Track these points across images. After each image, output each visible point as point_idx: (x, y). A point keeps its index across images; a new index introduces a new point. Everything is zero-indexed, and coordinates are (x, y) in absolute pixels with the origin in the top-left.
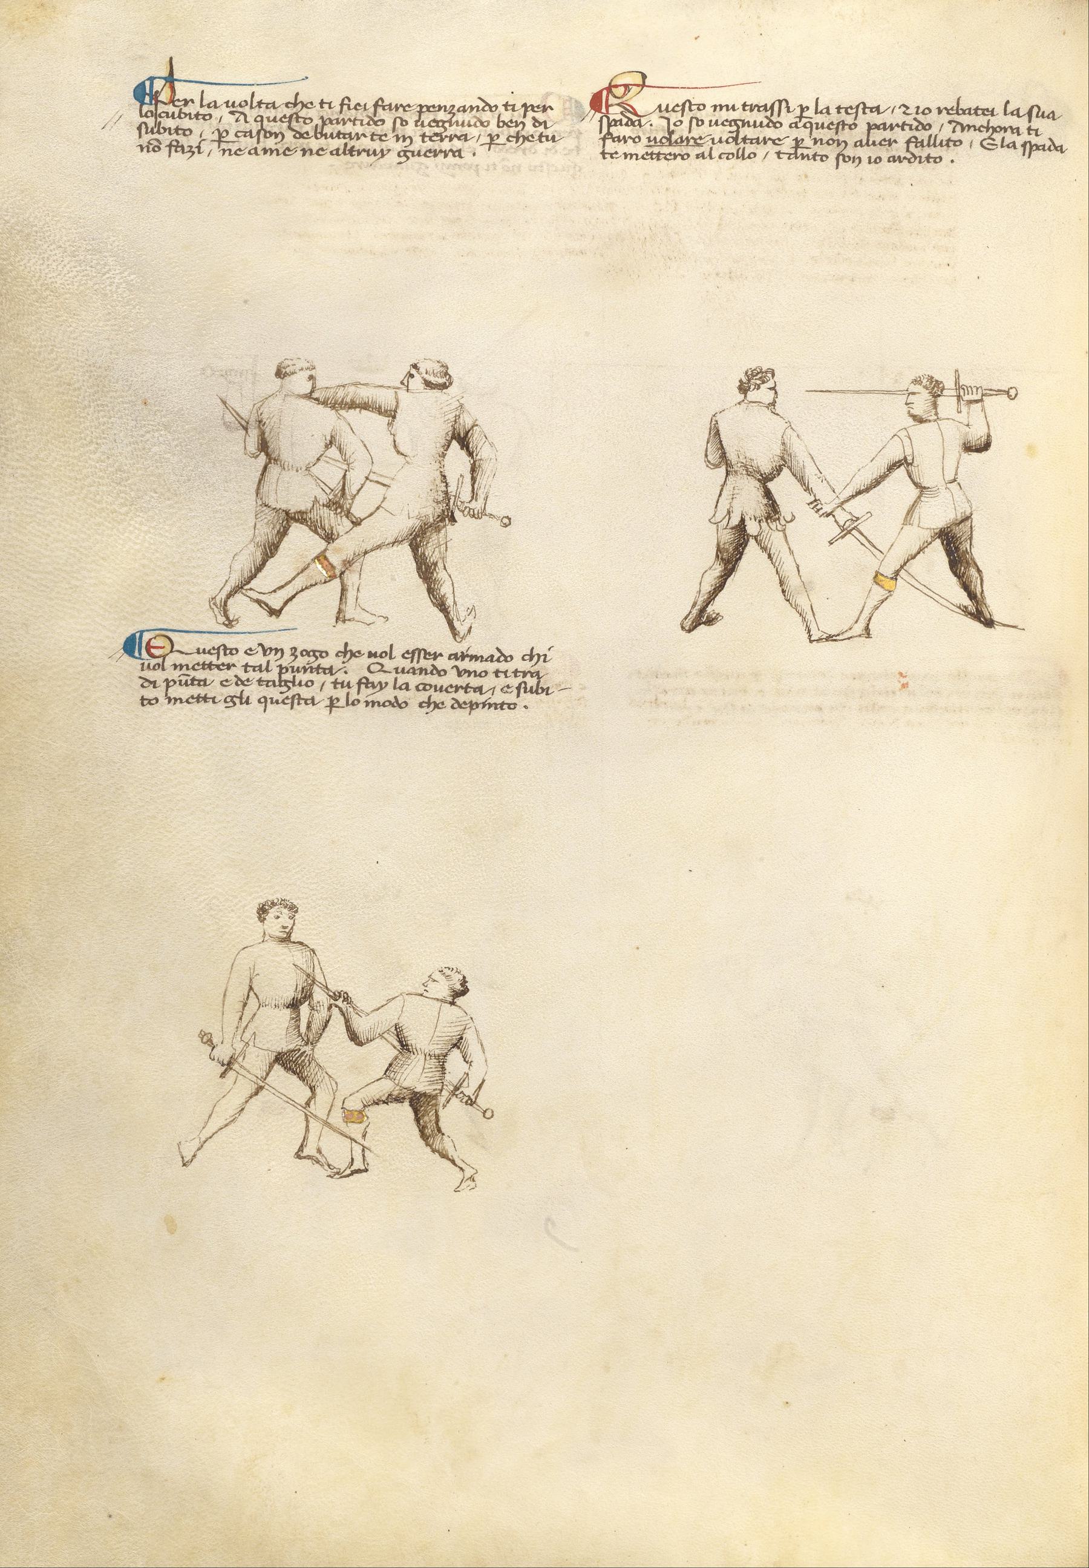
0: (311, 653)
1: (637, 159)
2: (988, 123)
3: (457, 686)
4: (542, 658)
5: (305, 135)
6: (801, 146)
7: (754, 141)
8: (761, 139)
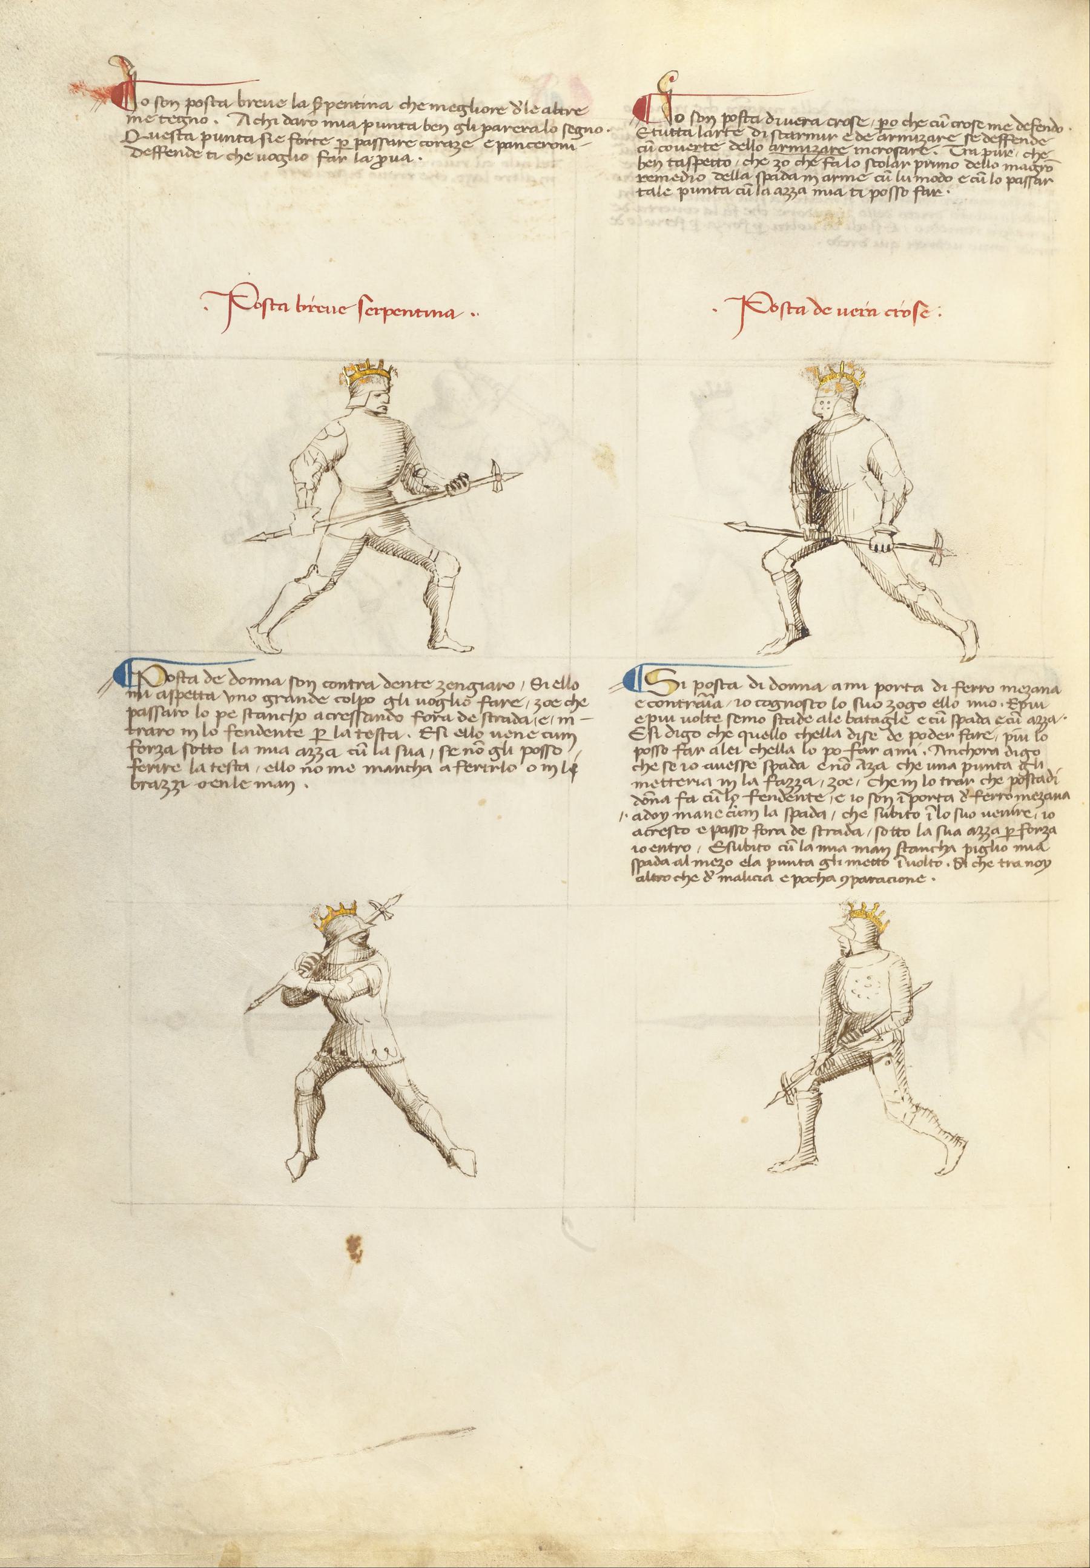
0: (280, 158)
1: (462, 689)
2: (263, 117)
3: (981, 686)
4: (273, 122)
5: (694, 878)
6: (324, 737)
7: (149, 732)
8: (827, 136)
